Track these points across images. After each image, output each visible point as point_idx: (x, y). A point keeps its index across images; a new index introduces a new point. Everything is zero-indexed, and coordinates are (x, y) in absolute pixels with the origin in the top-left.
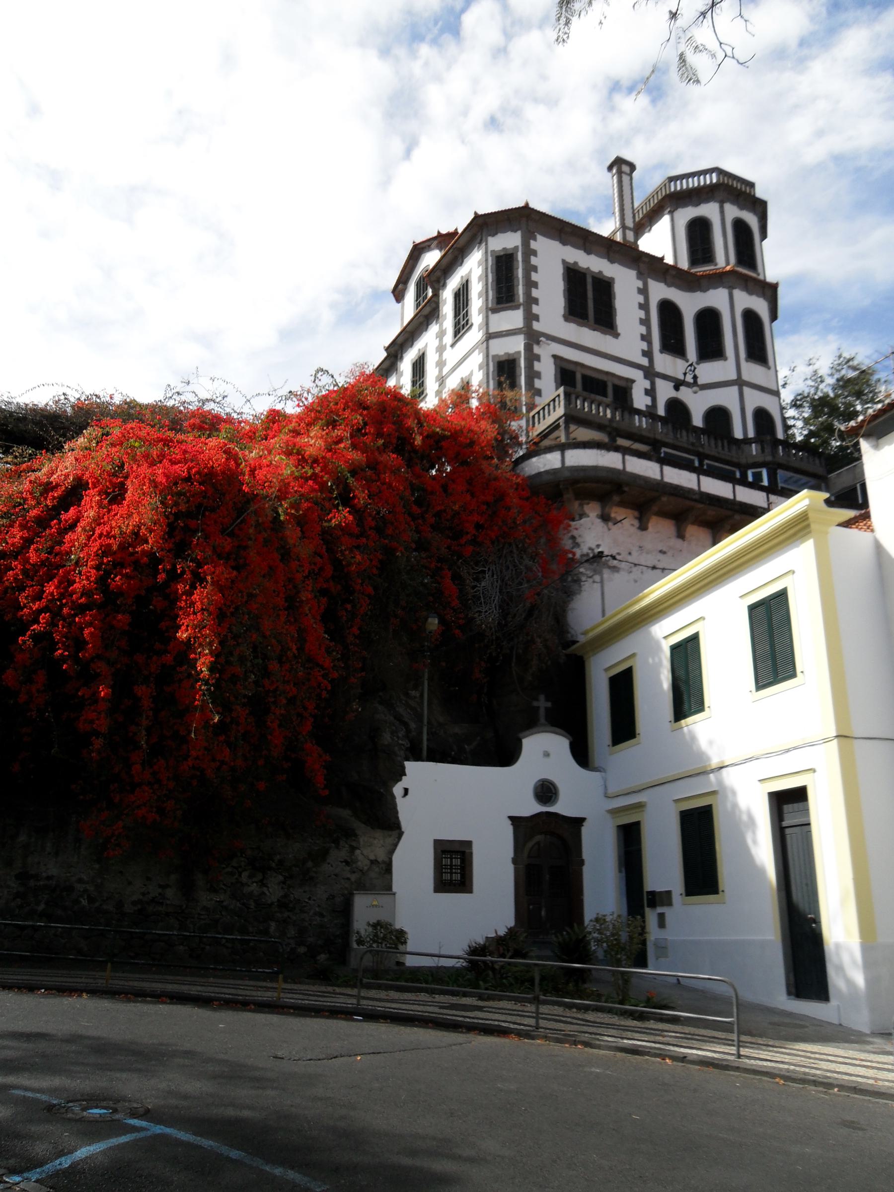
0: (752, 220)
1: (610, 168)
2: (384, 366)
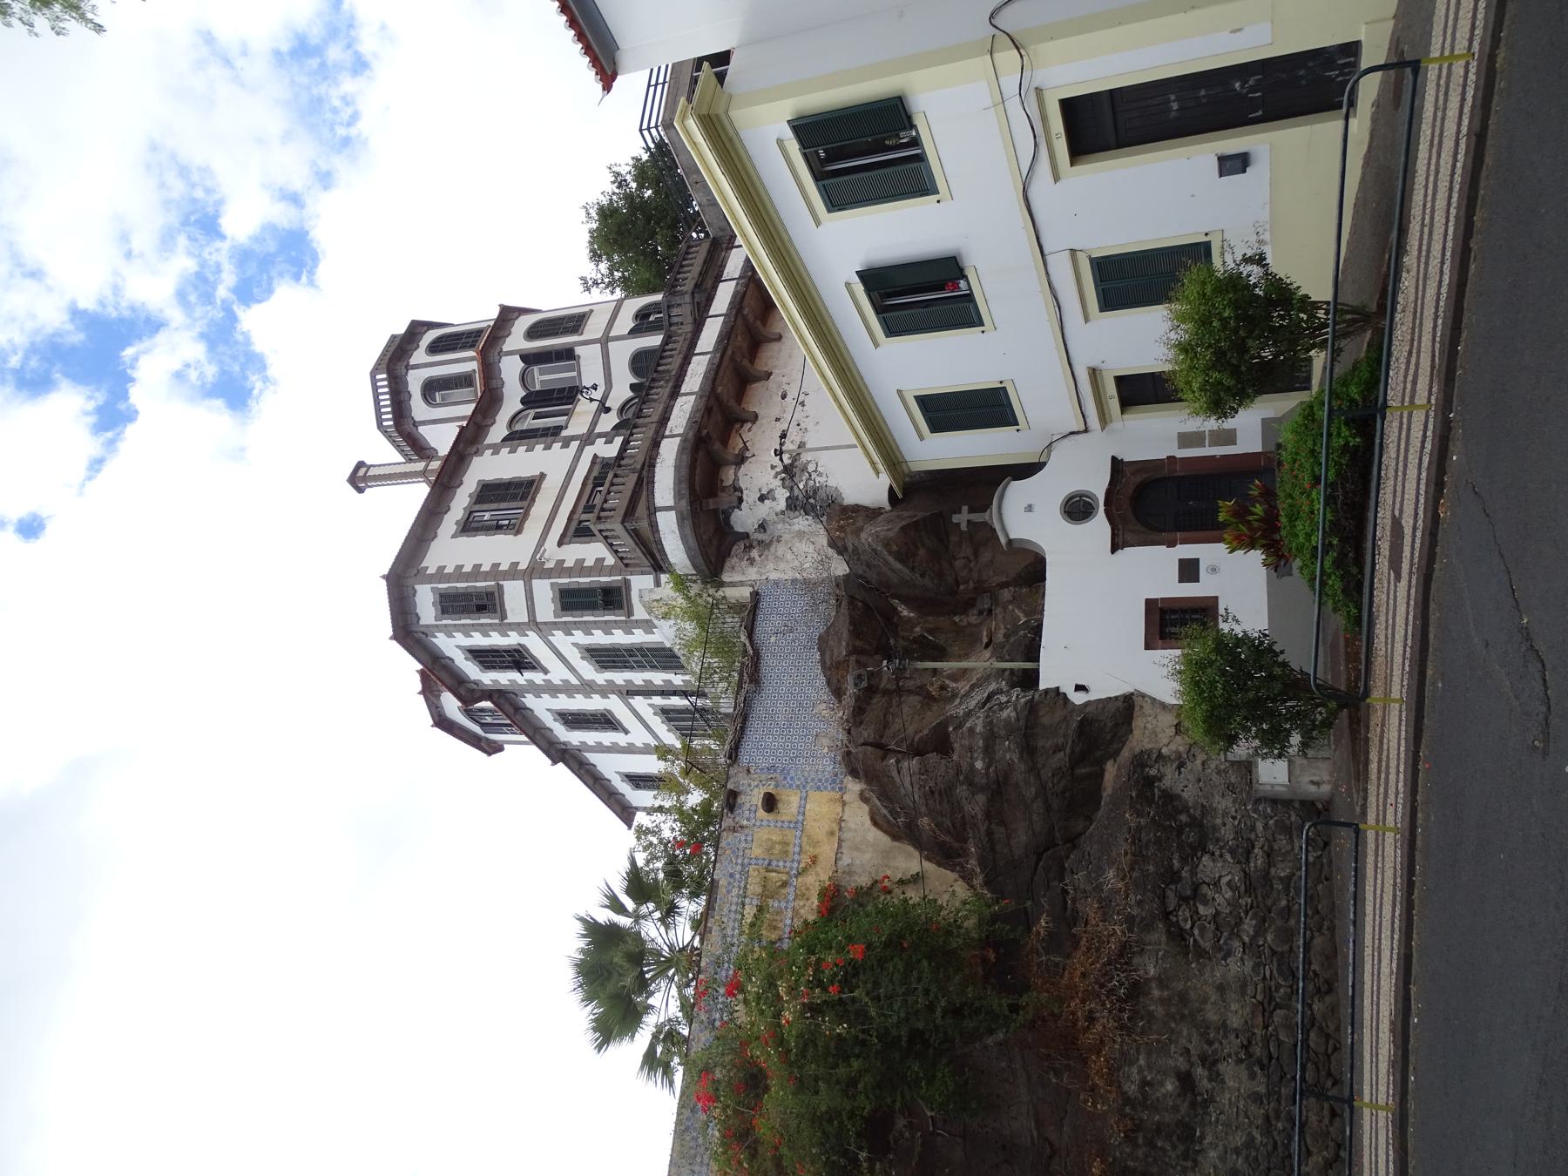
0: (430, 336)
1: (360, 490)
2: (591, 782)
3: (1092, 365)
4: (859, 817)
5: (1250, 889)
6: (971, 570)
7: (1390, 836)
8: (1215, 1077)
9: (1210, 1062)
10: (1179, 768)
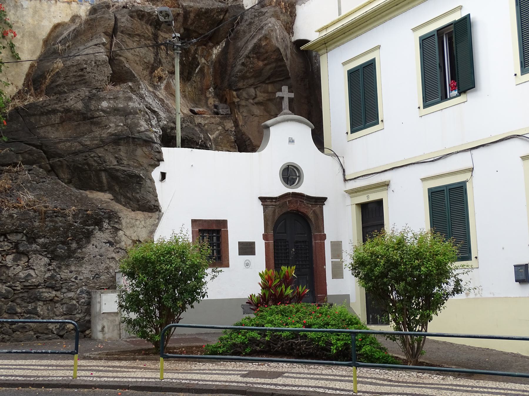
3: (392, 183)
5: (27, 289)
6: (247, 100)
7: (71, 373)
10: (109, 242)
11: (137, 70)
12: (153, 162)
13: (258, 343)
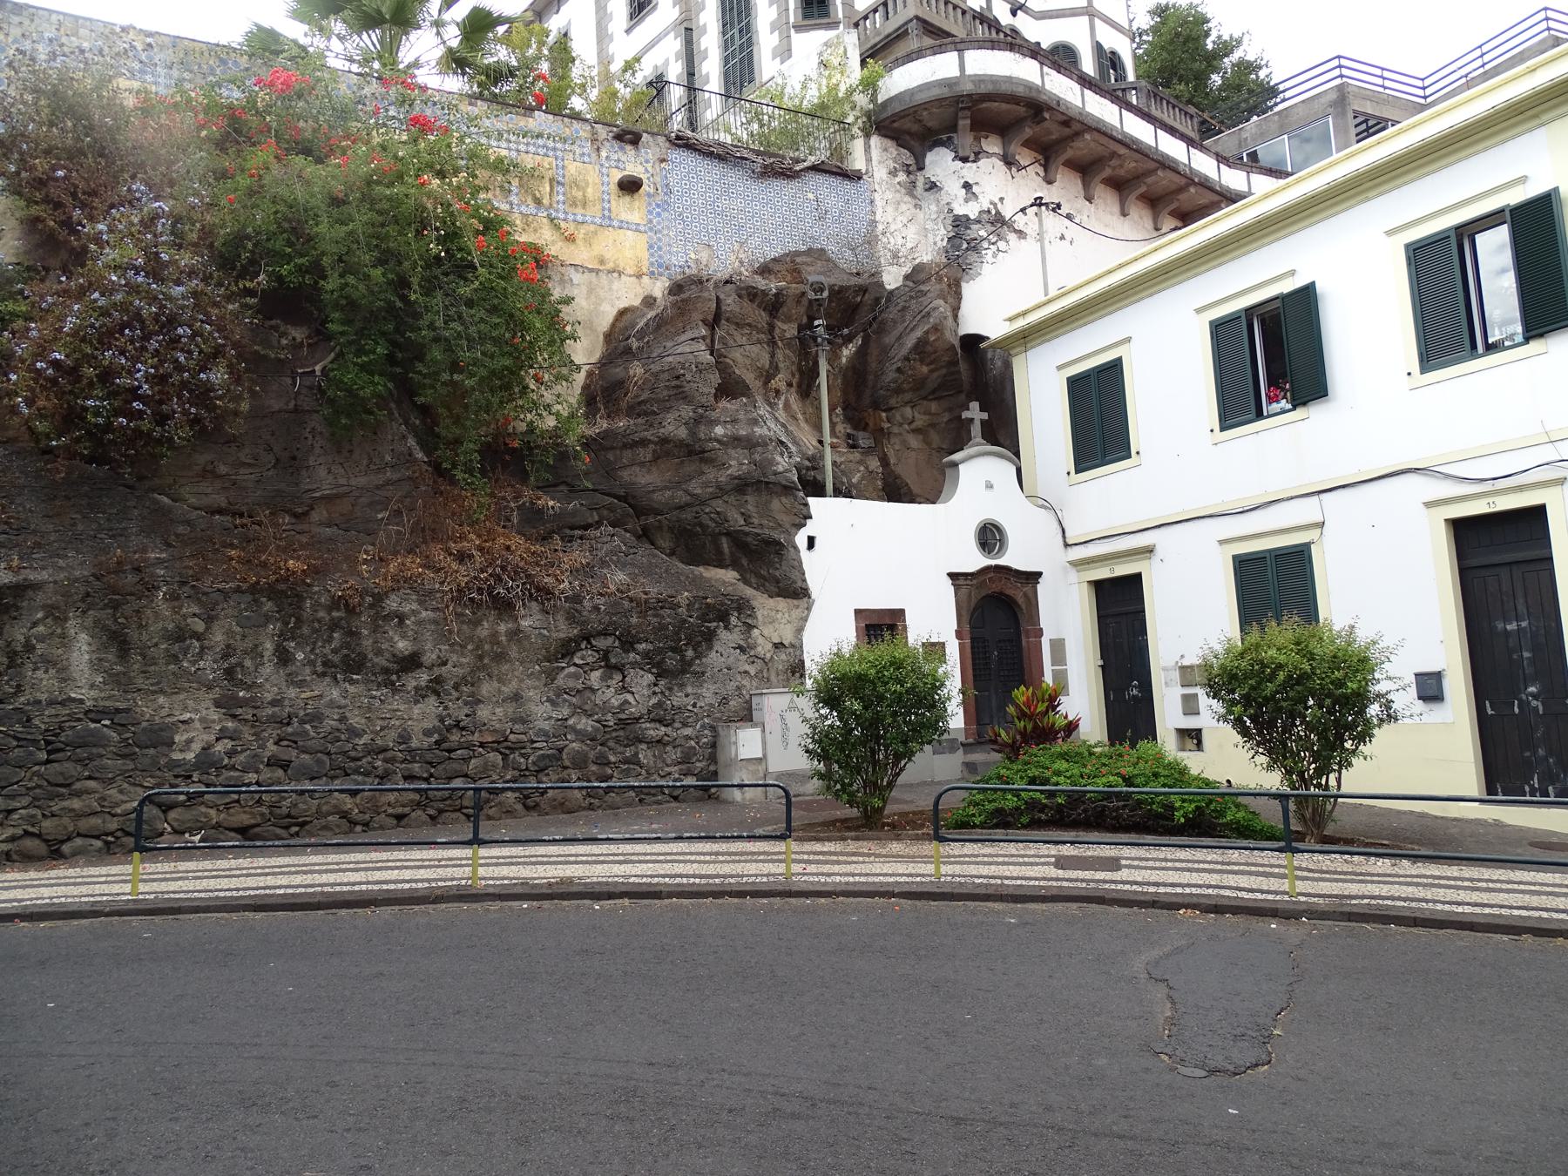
3: (1158, 549)
4: (627, 294)
5: (623, 723)
6: (901, 425)
7: (781, 868)
8: (420, 694)
9: (435, 687)
10: (740, 647)
11: (749, 377)
12: (797, 521)
13: (1043, 808)
